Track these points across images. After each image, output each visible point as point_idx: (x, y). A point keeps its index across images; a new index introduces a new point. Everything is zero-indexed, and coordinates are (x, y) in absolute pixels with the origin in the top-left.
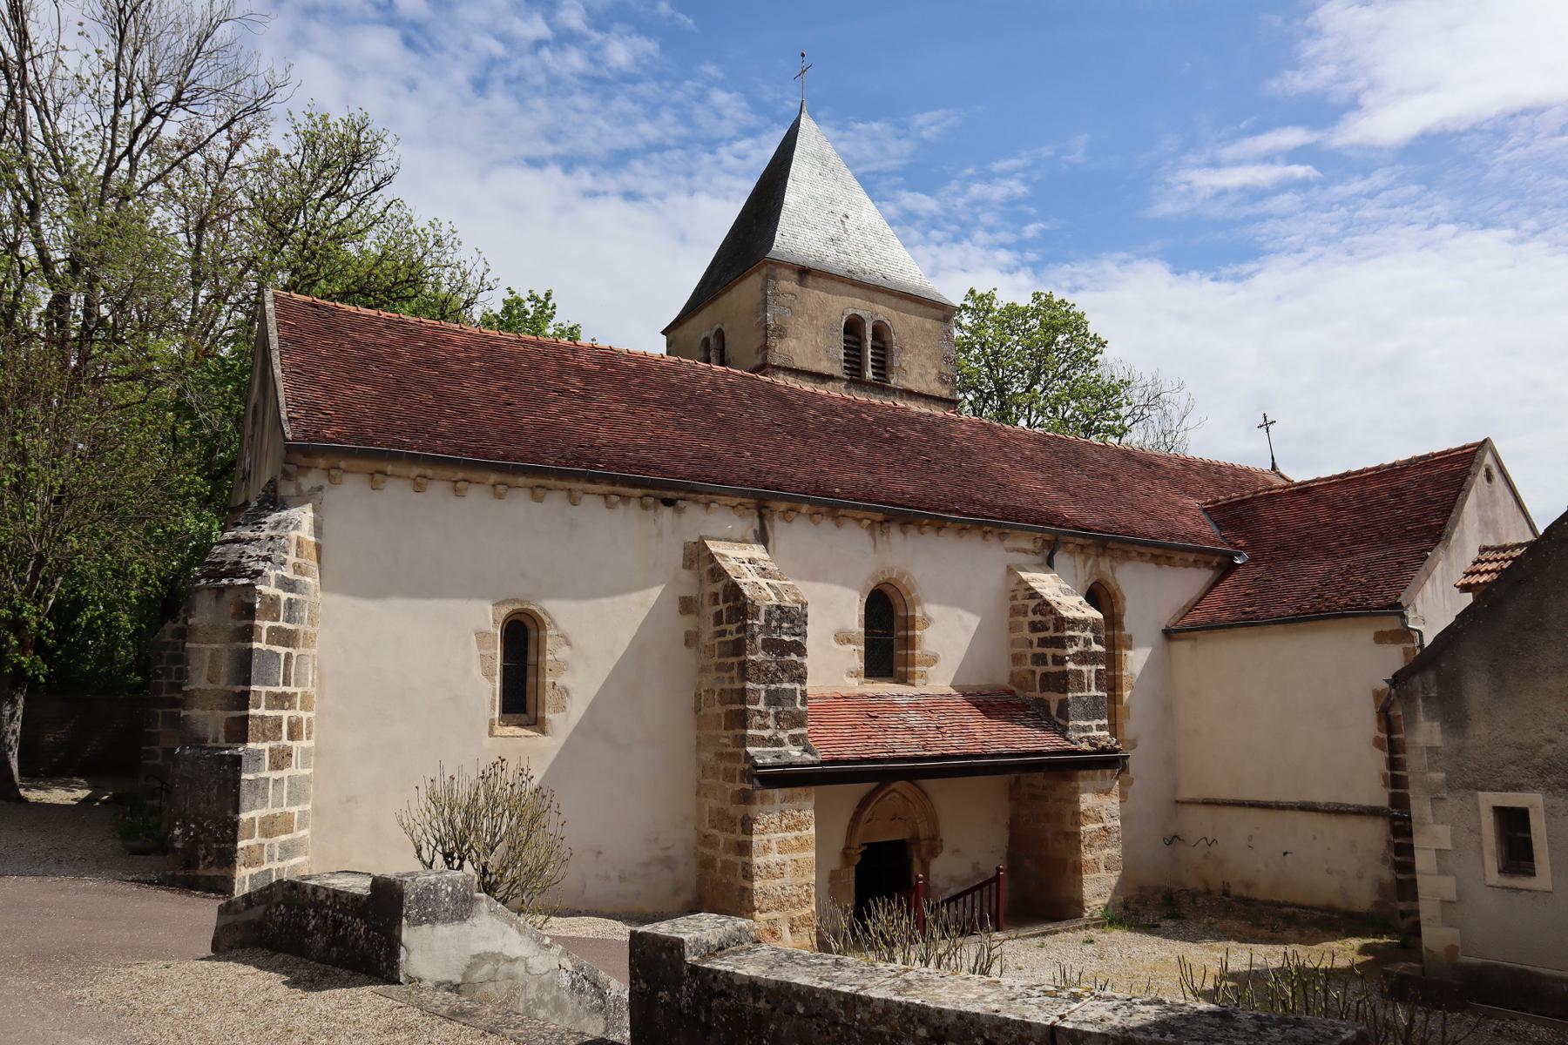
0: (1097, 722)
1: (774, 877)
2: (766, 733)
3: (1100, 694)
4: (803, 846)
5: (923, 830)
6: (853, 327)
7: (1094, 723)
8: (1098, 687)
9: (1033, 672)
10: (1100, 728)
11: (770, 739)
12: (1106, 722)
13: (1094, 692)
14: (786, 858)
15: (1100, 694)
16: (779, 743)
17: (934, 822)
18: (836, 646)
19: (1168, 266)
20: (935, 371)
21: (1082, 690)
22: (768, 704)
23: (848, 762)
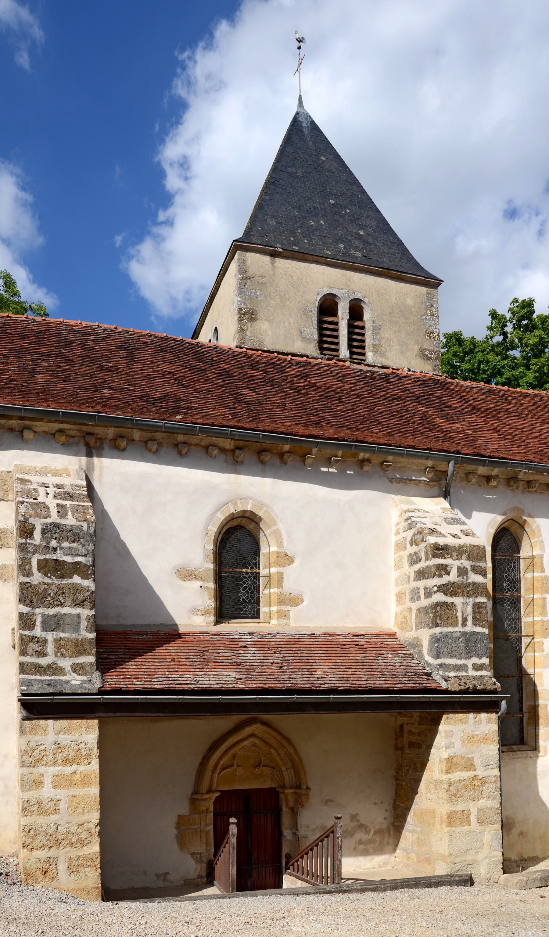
0: (475, 660)
1: (47, 813)
2: (44, 661)
3: (478, 629)
4: (84, 782)
5: (288, 776)
6: (327, 307)
7: (470, 662)
8: (476, 621)
9: (411, 609)
10: (477, 668)
11: (49, 666)
12: (485, 660)
13: (470, 627)
14: (60, 794)
15: (478, 629)
16: (59, 671)
17: (297, 767)
18: (180, 582)
19: (164, 182)
20: (416, 347)
21: (455, 624)
22: (46, 627)
23: (136, 692)
